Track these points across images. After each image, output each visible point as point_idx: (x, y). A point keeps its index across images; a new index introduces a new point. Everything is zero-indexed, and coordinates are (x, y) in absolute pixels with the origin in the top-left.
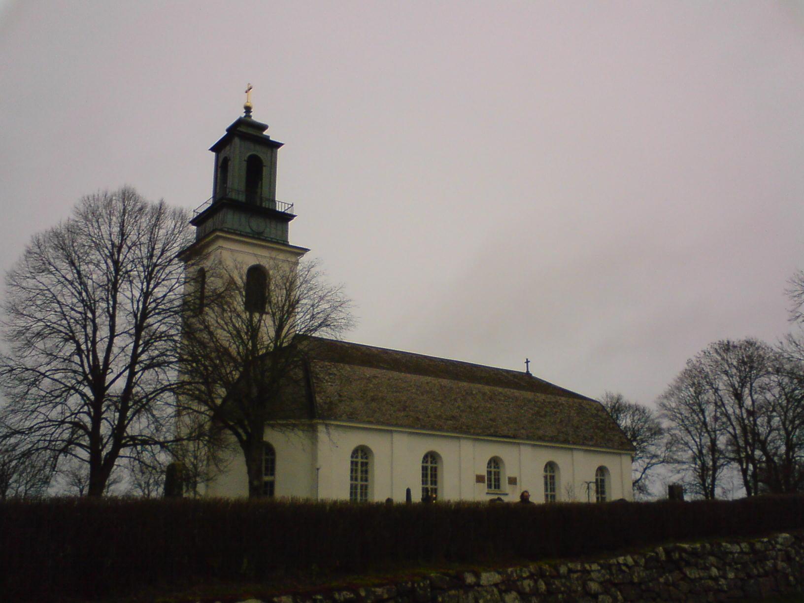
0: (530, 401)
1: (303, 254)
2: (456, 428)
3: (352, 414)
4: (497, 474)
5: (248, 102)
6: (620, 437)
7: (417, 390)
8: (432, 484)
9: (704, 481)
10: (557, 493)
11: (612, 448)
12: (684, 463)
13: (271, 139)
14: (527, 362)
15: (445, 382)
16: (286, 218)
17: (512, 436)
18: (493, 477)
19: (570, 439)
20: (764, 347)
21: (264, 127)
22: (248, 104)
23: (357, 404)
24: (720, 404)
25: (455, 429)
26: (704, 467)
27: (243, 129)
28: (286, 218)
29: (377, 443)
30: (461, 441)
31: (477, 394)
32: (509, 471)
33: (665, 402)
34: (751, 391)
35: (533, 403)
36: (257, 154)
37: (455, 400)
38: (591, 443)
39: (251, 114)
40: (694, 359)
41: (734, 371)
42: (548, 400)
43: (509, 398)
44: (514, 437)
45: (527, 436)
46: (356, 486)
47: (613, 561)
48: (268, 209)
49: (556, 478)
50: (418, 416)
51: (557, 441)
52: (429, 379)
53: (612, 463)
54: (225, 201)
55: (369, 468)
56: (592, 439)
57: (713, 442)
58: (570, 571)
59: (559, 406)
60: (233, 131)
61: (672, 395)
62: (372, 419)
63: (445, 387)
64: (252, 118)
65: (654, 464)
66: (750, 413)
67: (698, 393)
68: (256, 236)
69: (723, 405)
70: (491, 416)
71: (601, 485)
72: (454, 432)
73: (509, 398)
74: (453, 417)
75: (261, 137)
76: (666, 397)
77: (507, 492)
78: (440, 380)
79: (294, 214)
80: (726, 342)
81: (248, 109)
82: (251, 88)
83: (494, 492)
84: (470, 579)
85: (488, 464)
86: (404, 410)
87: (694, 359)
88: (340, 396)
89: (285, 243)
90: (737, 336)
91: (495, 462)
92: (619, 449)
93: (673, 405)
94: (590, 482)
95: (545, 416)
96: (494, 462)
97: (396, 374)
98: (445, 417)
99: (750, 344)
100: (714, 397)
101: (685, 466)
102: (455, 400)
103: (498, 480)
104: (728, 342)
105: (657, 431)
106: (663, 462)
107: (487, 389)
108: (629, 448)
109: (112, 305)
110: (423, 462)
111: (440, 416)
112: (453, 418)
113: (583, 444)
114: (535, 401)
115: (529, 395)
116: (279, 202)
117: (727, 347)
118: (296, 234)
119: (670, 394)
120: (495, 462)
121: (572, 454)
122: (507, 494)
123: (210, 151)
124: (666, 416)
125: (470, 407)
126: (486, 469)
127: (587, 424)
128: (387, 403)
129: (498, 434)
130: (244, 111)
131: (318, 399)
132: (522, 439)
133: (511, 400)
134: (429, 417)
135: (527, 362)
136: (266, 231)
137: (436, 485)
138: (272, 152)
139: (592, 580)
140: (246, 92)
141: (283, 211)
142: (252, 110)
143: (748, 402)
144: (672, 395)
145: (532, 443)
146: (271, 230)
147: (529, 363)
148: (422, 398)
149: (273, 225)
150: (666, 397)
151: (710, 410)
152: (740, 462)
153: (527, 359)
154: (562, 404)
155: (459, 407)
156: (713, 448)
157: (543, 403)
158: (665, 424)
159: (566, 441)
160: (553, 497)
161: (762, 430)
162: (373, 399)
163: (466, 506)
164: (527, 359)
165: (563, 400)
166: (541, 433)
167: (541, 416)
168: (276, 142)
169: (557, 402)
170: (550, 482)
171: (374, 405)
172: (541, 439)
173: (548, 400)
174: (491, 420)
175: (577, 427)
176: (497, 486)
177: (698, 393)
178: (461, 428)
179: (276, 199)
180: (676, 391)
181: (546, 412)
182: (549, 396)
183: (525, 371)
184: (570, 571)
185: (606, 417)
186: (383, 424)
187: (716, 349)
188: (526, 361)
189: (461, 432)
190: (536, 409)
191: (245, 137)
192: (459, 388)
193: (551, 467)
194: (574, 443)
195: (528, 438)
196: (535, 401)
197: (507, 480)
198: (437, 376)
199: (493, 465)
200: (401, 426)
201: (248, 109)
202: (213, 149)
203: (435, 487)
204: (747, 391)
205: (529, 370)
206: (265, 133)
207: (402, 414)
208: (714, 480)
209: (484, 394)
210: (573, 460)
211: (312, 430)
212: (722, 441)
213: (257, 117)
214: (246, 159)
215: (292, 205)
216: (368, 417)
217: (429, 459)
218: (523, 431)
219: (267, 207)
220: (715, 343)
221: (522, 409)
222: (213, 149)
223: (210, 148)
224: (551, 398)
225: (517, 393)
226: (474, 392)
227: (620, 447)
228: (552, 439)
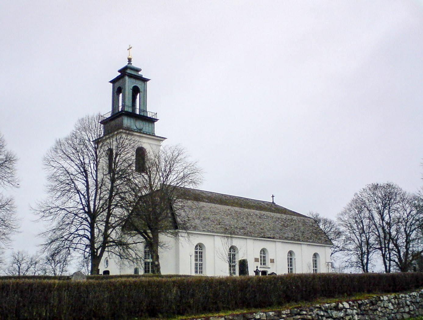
0: (279, 218)
1: (162, 141)
2: (245, 234)
3: (195, 227)
4: (264, 257)
5: (129, 55)
6: (325, 238)
7: (224, 213)
8: (199, 261)
9: (362, 261)
10: (318, 268)
11: (321, 243)
12: (351, 251)
13: (143, 77)
14: (273, 197)
15: (237, 209)
16: (152, 121)
17: (272, 237)
18: (262, 259)
19: (300, 238)
20: (397, 187)
21: (138, 70)
22: (130, 57)
23: (197, 221)
24: (371, 218)
25: (245, 234)
26: (363, 254)
27: (129, 71)
28: (152, 121)
29: (207, 241)
30: (247, 240)
31: (253, 215)
32: (270, 256)
33: (342, 217)
34: (389, 212)
35: (281, 219)
36: (137, 85)
37: (243, 218)
38: (311, 241)
39: (132, 62)
40: (358, 193)
41: (380, 200)
42: (288, 218)
43: (269, 217)
44: (273, 238)
45: (280, 238)
46: (197, 264)
47: (411, 294)
48: (144, 116)
49: (318, 261)
50: (226, 227)
51: (295, 240)
52: (229, 207)
53: (319, 250)
54: (123, 112)
55: (203, 255)
56: (311, 238)
57: (368, 240)
58: (402, 297)
59: (293, 221)
60: (123, 71)
61: (345, 213)
62: (204, 229)
63: (237, 211)
64: (132, 65)
65: (336, 251)
66: (389, 224)
67: (360, 212)
68: (139, 131)
69: (373, 218)
70: (261, 227)
71: (290, 262)
72: (244, 236)
73: (269, 217)
74: (243, 228)
75: (138, 76)
76: (342, 214)
77: (269, 267)
78: (234, 208)
79: (158, 119)
80: (376, 184)
81: (130, 60)
82: (131, 48)
83: (263, 267)
84: (382, 298)
85: (196, 247)
86: (219, 224)
87: (358, 193)
88: (188, 217)
89: (154, 134)
90: (382, 182)
91: (263, 251)
92: (324, 244)
93: (346, 219)
94: (329, 262)
95: (287, 227)
96: (290, 253)
97: (213, 205)
98: (239, 228)
99: (389, 185)
100: (369, 215)
101: (351, 252)
102: (243, 218)
103: (264, 260)
104: (378, 185)
105: (339, 234)
106: (341, 250)
107: (257, 212)
108: (329, 243)
109: (390, 242)
110: (195, 249)
111: (237, 227)
112: (243, 228)
113: (307, 241)
114: (281, 219)
115: (279, 215)
116: (150, 112)
117: (376, 187)
118: (159, 129)
119: (344, 213)
120: (263, 251)
121: (275, 244)
122: (269, 268)
123: (109, 83)
124: (342, 225)
125: (251, 222)
126: (194, 250)
127: (308, 230)
128: (211, 221)
129: (266, 237)
130: (128, 60)
131: (178, 219)
132: (277, 239)
133: (270, 218)
134: (231, 228)
135: (273, 197)
136: (144, 128)
137: (202, 261)
138: (144, 83)
139: (407, 300)
140: (128, 50)
141: (150, 116)
142: (132, 60)
143: (387, 218)
144: (345, 213)
145: (282, 241)
146: (146, 127)
147: (274, 197)
148: (227, 217)
149: (147, 124)
150: (342, 214)
151: (366, 222)
152: (381, 249)
153: (273, 195)
154: (295, 220)
155: (245, 222)
156: (368, 243)
157: (285, 220)
158: (342, 229)
159: (299, 240)
160: (316, 270)
161: (394, 233)
162: (204, 219)
163: (304, 276)
164: (273, 195)
165: (295, 218)
166: (286, 235)
167: (285, 227)
168: (145, 79)
169: (292, 219)
170: (290, 262)
171: (205, 222)
172: (286, 239)
173: (287, 218)
174: (261, 229)
175: (303, 232)
176: (264, 264)
177: (360, 212)
178: (247, 233)
179: (147, 110)
180: (348, 211)
181: (287, 224)
182: (288, 216)
183: (272, 202)
184: (402, 297)
185: (317, 227)
186: (210, 232)
187: (369, 188)
188: (272, 196)
189: (247, 236)
190: (282, 223)
191: (131, 76)
192: (244, 212)
193: (291, 253)
194: (303, 241)
195: (280, 238)
196: (281, 219)
197: (269, 260)
198: (232, 206)
199: (262, 252)
200: (217, 232)
201: (130, 60)
202: (111, 82)
203: (202, 263)
204: (386, 211)
205: (274, 201)
206: (140, 73)
207: (219, 226)
208: (368, 259)
209: (256, 215)
210: (301, 249)
211: (176, 235)
212: (372, 240)
213: (134, 64)
214: (132, 88)
215: (157, 114)
216: (203, 228)
217: (198, 247)
218: (278, 235)
219: (143, 115)
220: (370, 185)
221: (276, 223)
222: (111, 82)
223: (110, 81)
224: (289, 217)
225: (272, 214)
226: (252, 214)
227: (325, 243)
228: (292, 239)
